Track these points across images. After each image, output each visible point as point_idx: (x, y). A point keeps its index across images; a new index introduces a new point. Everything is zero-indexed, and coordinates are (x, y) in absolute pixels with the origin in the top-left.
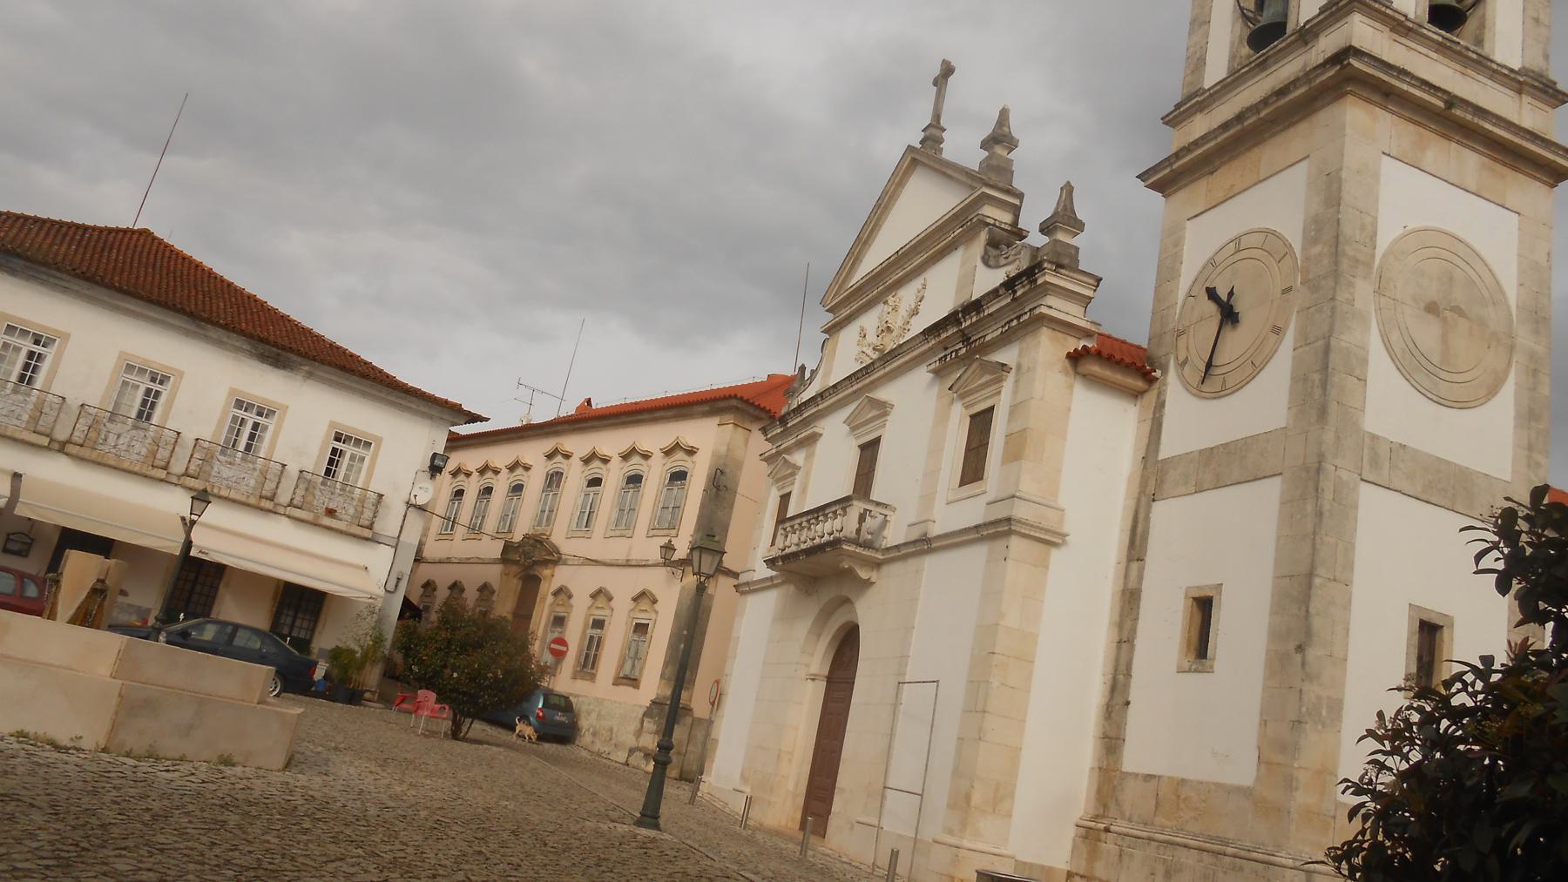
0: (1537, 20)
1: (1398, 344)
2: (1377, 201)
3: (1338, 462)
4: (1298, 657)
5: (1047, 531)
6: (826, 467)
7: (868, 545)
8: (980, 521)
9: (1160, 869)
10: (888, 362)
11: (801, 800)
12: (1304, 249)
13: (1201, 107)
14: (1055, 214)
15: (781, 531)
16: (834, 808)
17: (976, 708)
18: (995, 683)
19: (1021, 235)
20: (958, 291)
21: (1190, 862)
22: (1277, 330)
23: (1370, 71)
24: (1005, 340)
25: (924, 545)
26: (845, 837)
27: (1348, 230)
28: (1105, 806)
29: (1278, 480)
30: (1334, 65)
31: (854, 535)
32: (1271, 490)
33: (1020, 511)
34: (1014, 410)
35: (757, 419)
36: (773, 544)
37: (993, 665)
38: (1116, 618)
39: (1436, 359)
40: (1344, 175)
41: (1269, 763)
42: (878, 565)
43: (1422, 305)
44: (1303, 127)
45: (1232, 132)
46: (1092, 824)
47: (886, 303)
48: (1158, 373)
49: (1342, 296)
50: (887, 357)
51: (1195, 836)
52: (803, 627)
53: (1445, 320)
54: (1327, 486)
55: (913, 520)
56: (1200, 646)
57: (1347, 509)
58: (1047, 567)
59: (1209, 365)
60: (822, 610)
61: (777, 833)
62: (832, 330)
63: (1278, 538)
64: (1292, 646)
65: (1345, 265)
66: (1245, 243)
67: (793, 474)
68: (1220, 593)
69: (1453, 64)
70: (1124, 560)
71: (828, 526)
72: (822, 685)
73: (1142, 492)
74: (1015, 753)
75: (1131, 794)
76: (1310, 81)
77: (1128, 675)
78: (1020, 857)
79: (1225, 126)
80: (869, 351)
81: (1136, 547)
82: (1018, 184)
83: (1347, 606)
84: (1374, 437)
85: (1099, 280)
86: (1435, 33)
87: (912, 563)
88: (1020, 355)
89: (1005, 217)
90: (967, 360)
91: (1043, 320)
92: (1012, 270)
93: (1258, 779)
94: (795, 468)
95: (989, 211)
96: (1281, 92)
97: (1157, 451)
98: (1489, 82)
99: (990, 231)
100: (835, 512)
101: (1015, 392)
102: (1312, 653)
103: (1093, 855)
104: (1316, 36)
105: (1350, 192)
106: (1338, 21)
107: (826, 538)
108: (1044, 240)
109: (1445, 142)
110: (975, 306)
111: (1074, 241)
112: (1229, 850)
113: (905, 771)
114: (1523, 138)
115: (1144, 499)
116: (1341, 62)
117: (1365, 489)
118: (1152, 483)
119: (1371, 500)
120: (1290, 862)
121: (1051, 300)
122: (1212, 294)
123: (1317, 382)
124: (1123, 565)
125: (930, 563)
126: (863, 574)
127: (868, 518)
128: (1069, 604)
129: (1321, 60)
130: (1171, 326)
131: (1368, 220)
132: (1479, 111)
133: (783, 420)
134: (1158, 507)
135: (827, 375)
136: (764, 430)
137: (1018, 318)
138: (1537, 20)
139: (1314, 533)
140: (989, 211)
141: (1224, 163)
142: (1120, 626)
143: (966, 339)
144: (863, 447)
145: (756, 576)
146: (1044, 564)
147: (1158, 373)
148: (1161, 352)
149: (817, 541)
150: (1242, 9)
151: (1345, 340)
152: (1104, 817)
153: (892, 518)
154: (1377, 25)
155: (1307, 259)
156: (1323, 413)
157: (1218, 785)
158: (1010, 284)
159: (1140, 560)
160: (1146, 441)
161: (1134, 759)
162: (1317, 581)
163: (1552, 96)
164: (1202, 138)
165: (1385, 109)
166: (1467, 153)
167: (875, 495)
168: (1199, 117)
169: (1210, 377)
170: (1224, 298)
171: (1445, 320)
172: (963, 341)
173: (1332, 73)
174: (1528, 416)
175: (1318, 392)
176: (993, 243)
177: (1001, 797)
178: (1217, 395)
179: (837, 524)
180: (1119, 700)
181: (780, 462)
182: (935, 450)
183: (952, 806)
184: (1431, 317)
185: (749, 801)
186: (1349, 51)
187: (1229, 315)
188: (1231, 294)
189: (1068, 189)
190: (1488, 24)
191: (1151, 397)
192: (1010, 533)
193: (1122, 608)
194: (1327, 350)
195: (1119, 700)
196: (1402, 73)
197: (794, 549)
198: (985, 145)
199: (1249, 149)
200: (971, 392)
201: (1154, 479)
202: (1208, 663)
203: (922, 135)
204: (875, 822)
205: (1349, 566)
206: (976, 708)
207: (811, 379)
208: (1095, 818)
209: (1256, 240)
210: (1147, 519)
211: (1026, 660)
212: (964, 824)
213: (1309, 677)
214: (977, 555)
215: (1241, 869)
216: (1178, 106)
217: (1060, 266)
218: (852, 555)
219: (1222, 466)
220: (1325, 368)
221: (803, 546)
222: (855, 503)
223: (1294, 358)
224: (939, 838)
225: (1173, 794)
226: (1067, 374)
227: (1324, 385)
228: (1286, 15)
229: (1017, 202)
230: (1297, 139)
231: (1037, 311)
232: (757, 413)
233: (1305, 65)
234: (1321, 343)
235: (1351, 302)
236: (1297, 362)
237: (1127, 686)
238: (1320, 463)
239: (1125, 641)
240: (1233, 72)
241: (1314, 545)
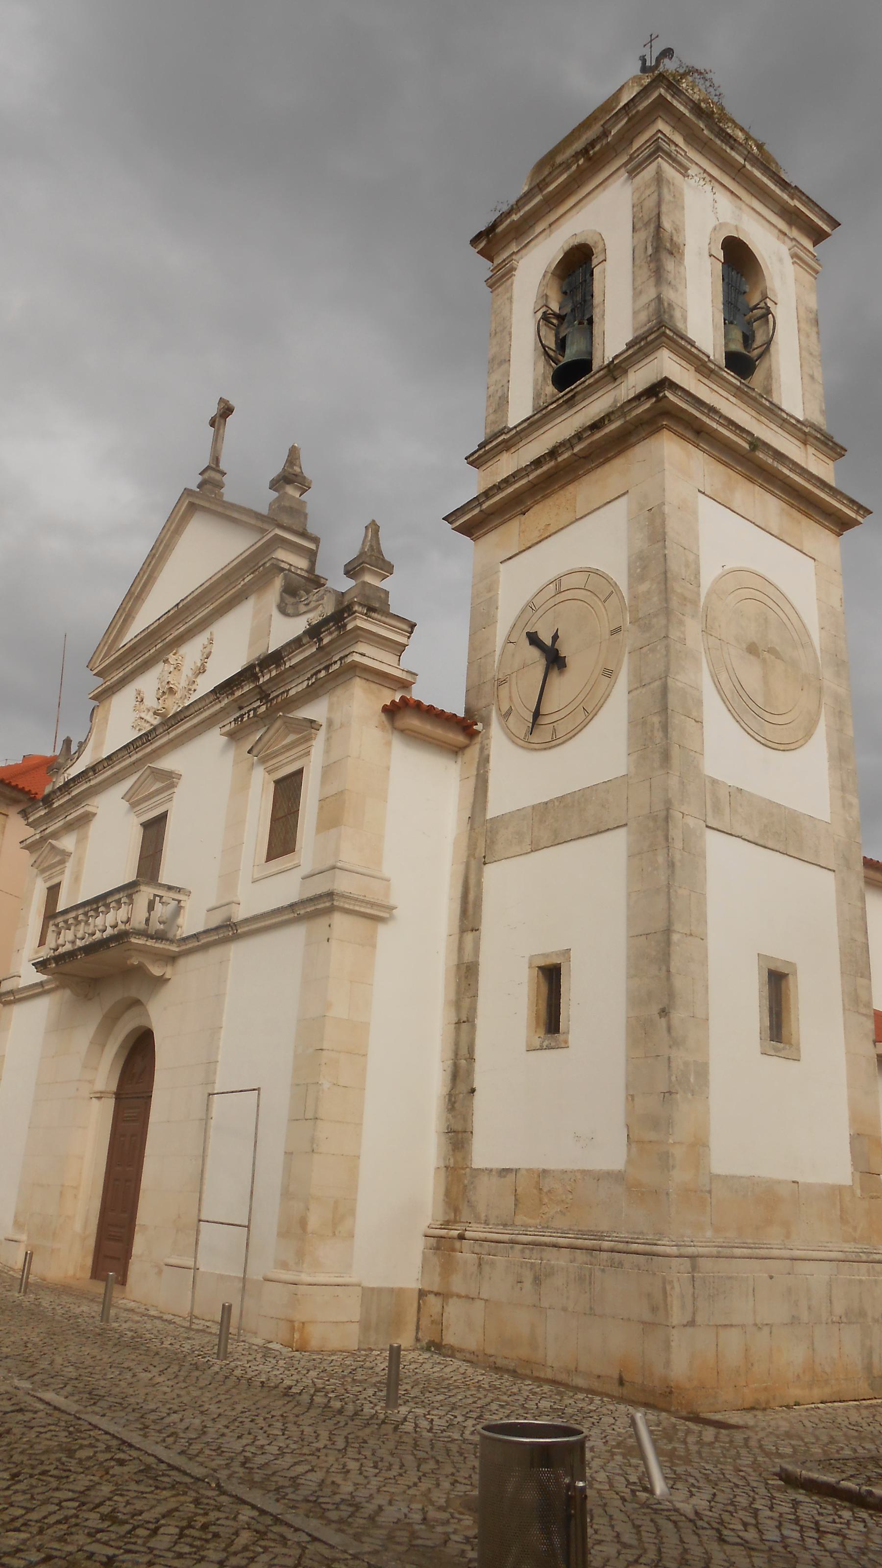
0: (812, 377)
1: (727, 688)
2: (697, 538)
3: (684, 809)
4: (663, 1021)
5: (373, 905)
6: (104, 850)
7: (160, 936)
8: (294, 899)
9: (528, 1277)
10: (173, 727)
11: (91, 1242)
12: (630, 587)
13: (507, 446)
14: (362, 554)
15: (52, 928)
16: (138, 1247)
17: (305, 1114)
18: (326, 1085)
19: (316, 582)
20: (251, 644)
21: (562, 1263)
22: (608, 673)
23: (684, 406)
24: (311, 694)
25: (227, 931)
26: (153, 1283)
27: (674, 566)
28: (456, 1210)
29: (623, 831)
30: (649, 397)
31: (143, 926)
32: (614, 847)
33: (343, 884)
34: (327, 771)
35: (15, 802)
36: (42, 943)
37: (320, 1063)
38: (452, 996)
39: (760, 700)
40: (667, 509)
41: (640, 1142)
42: (172, 959)
43: (744, 646)
44: (618, 463)
45: (545, 468)
46: (443, 1232)
47: (166, 661)
48: (479, 727)
49: (674, 634)
50: (170, 722)
51: (564, 1233)
52: (83, 1037)
53: (764, 661)
54: (676, 833)
55: (213, 903)
56: (551, 1020)
57: (696, 857)
58: (374, 946)
59: (537, 714)
60: (105, 1017)
61: (62, 1289)
62: (103, 696)
63: (629, 895)
64: (655, 1009)
65: (675, 602)
66: (566, 583)
67: (62, 862)
68: (569, 960)
69: (749, 410)
70: (456, 930)
71: (110, 918)
72: (110, 1103)
73: (471, 854)
74: (352, 1162)
75: (485, 1194)
76: (624, 415)
77: (471, 1058)
78: (366, 1284)
79: (537, 463)
80: (149, 717)
81: (469, 915)
82: (311, 529)
83: (704, 962)
84: (714, 782)
85: (413, 626)
86: (731, 377)
87: (214, 954)
88: (331, 708)
89: (300, 563)
90: (268, 719)
91: (355, 669)
92: (315, 617)
93: (629, 1161)
94: (65, 855)
95: (282, 555)
96: (596, 426)
97: (484, 809)
98: (779, 430)
99: (285, 577)
100: (118, 902)
101: (327, 751)
102: (678, 1016)
103: (448, 1268)
104: (625, 372)
105: (673, 526)
106: (646, 356)
107: (110, 931)
108: (351, 583)
109: (751, 485)
110: (275, 658)
111: (384, 585)
112: (606, 1245)
113: (223, 1197)
114: (814, 485)
115: (473, 863)
116: (656, 395)
117: (710, 833)
118: (481, 844)
119: (715, 844)
120: (674, 1250)
121: (362, 647)
122: (533, 639)
123: (657, 726)
124: (456, 937)
125: (236, 951)
126: (156, 971)
127: (158, 906)
128: (400, 984)
129: (632, 395)
130: (489, 676)
131: (691, 557)
132: (779, 456)
133: (47, 800)
134: (491, 873)
135: (99, 745)
136: (24, 814)
137: (327, 668)
138: (812, 377)
139: (669, 886)
140: (282, 555)
141: (537, 502)
142: (457, 1004)
143: (263, 695)
144: (146, 826)
145: (22, 983)
146: (370, 943)
147: (479, 727)
148: (482, 703)
149: (98, 935)
150: (544, 346)
151: (678, 681)
152: (455, 1222)
153: (187, 903)
154: (684, 363)
155: (635, 597)
156: (666, 757)
157: (584, 1172)
158: (314, 632)
159: (475, 929)
160: (471, 799)
161: (484, 1153)
162: (675, 937)
163: (832, 449)
164: (513, 475)
165: (697, 446)
166: (768, 496)
167: (165, 877)
168: (505, 457)
169: (538, 727)
170: (548, 642)
171: (764, 661)
172: (260, 698)
173: (647, 406)
174: (840, 756)
175: (658, 735)
176: (290, 591)
177: (341, 1216)
178: (548, 746)
179: (122, 914)
180: (462, 1088)
181: (46, 848)
182: (235, 822)
183: (284, 1233)
184: (752, 657)
185: (29, 1257)
186: (665, 383)
187: (555, 660)
188: (555, 637)
189: (374, 528)
190: (774, 375)
191: (474, 751)
192: (331, 910)
193: (458, 985)
194: (665, 690)
195: (462, 1088)
196: (712, 410)
197: (68, 947)
198: (275, 485)
199: (562, 487)
200: (276, 754)
201: (483, 840)
202: (560, 1037)
203: (199, 479)
204: (191, 1264)
205: (702, 919)
206: (305, 1114)
207: (80, 752)
208: (446, 1225)
209: (578, 580)
210: (479, 884)
211: (358, 1053)
212: (300, 1255)
213: (675, 1043)
214: (291, 940)
215: (621, 1264)
216: (481, 446)
217: (371, 609)
218: (141, 950)
219: (559, 821)
220: (664, 709)
221: (79, 944)
222: (143, 888)
223: (629, 701)
224: (271, 1275)
225: (534, 1188)
226: (383, 729)
227: (665, 727)
228: (591, 354)
229: (312, 546)
230: (612, 475)
231: (349, 660)
232: (14, 794)
233: (615, 401)
234: (657, 683)
235: (683, 641)
236: (633, 705)
237: (470, 1072)
238: (668, 810)
239: (464, 1021)
240: (538, 410)
241: (669, 899)
